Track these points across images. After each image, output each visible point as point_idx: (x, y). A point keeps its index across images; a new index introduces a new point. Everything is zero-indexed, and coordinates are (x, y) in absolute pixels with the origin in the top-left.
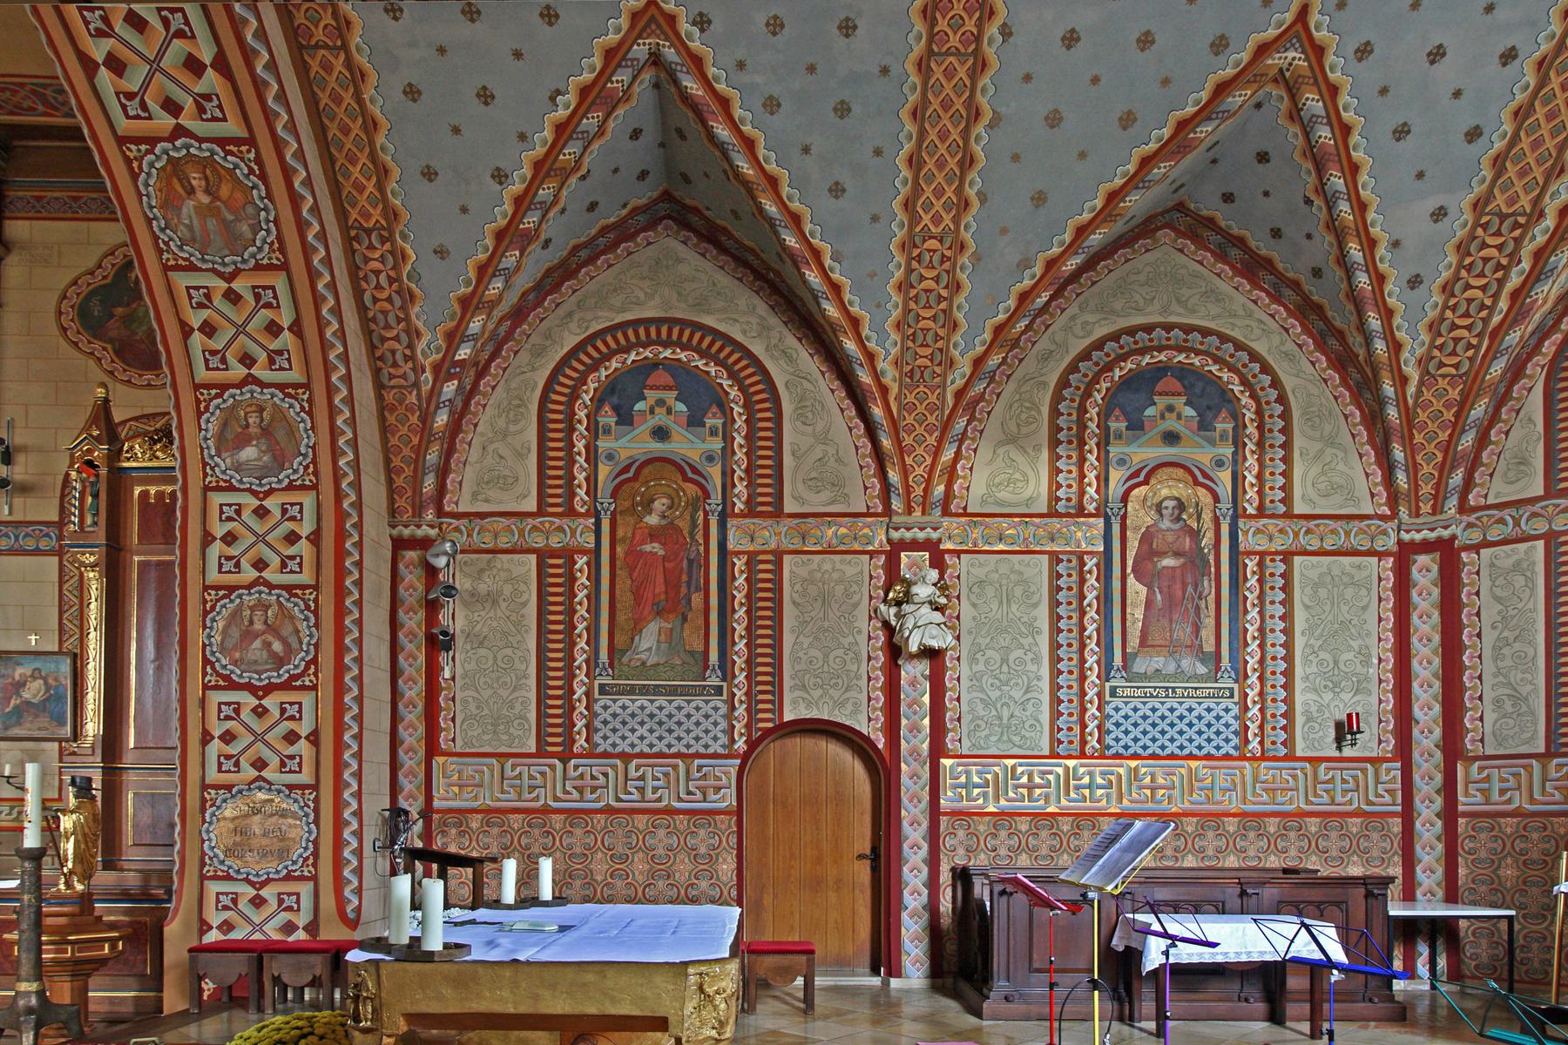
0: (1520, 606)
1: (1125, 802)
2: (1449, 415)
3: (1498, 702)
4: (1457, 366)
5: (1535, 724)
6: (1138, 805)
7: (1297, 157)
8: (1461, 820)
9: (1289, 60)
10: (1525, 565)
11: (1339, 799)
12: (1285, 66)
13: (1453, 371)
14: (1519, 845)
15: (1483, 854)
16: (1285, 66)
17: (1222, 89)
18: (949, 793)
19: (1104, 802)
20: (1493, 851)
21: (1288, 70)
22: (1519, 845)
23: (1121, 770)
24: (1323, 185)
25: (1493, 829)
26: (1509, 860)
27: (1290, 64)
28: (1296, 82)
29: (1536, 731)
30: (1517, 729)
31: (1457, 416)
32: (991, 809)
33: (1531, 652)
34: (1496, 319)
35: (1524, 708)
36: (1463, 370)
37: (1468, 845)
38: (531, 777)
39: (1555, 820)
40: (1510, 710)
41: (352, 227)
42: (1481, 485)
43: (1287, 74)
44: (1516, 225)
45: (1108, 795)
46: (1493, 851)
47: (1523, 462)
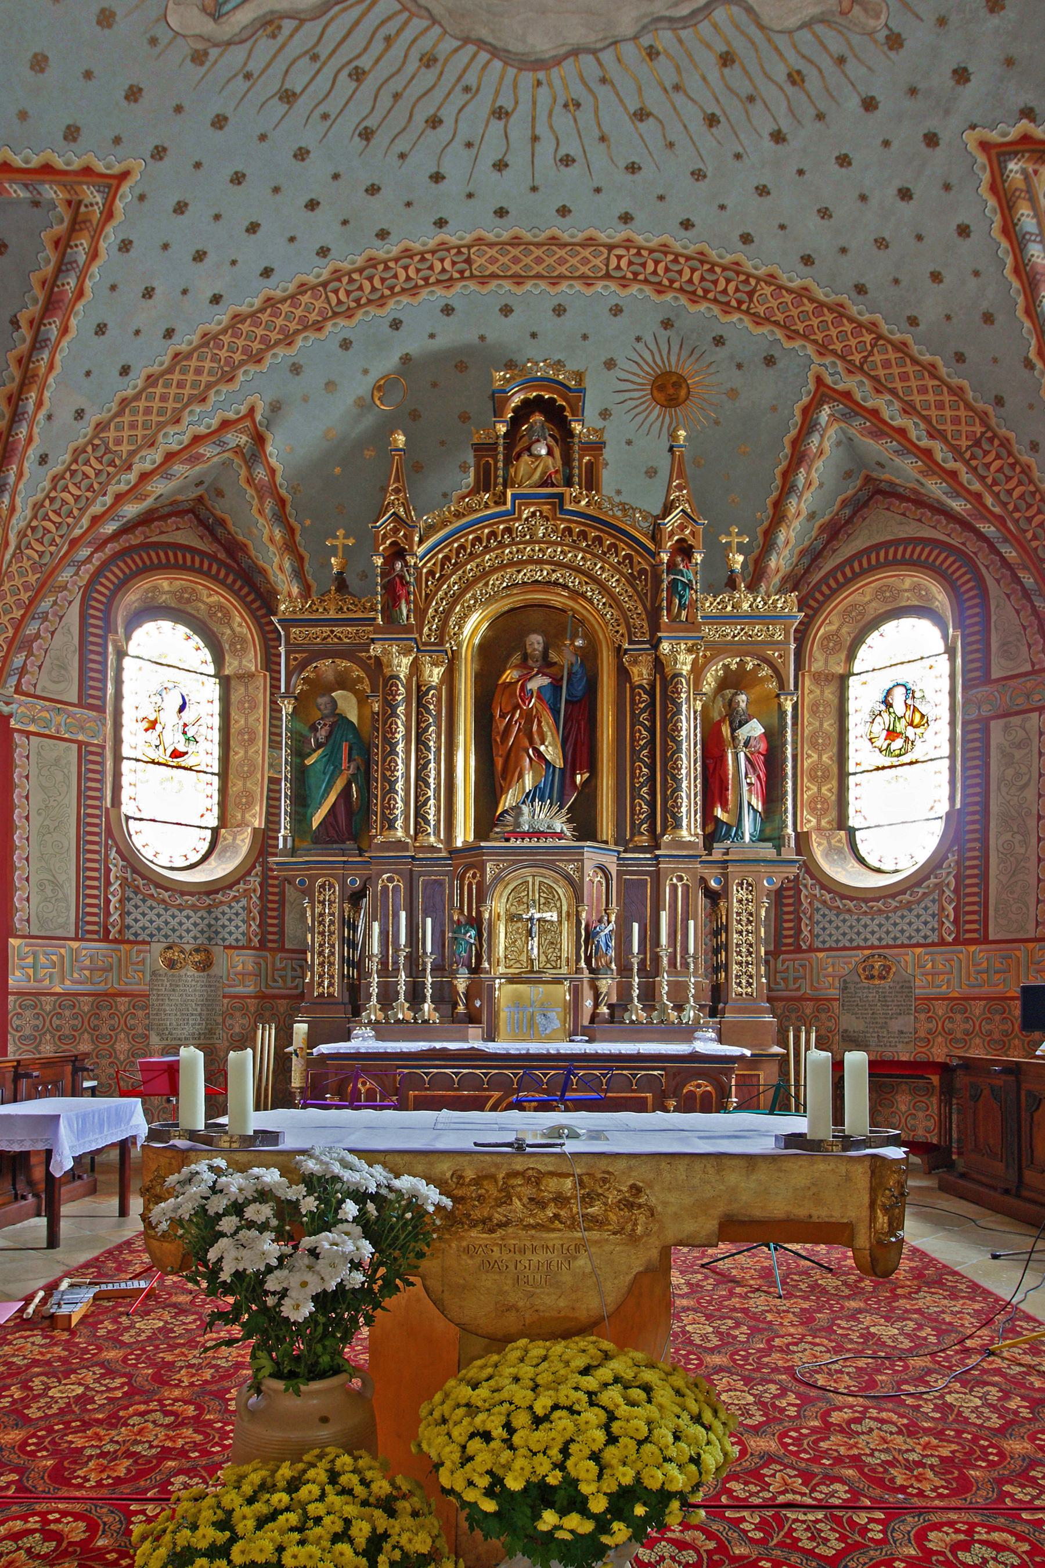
0: (59, 799)
1: (67, 982)
2: (25, 596)
3: (41, 885)
4: (41, 555)
5: (68, 910)
6: (977, 990)
7: (35, 279)
8: (11, 998)
9: (94, 201)
10: (64, 762)
11: (792, 986)
12: (86, 201)
13: (36, 556)
14: (56, 1022)
15: (28, 1031)
16: (86, 201)
17: (47, 170)
18: (17, 973)
19: (47, 982)
20: (36, 1028)
21: (86, 206)
22: (56, 1022)
23: (62, 951)
24: (41, 323)
25: (35, 1007)
26: (48, 1037)
27: (92, 205)
28: (84, 222)
29: (68, 917)
30: (55, 913)
31: (32, 600)
32: (58, 990)
33: (66, 844)
34: (78, 532)
35: (60, 895)
36: (44, 561)
37: (16, 1022)
38: (795, 970)
39: (82, 998)
40: (50, 894)
41: (757, 283)
42: (32, 673)
43: (83, 209)
44: (112, 463)
45: (51, 975)
46: (36, 1028)
47: (63, 667)
